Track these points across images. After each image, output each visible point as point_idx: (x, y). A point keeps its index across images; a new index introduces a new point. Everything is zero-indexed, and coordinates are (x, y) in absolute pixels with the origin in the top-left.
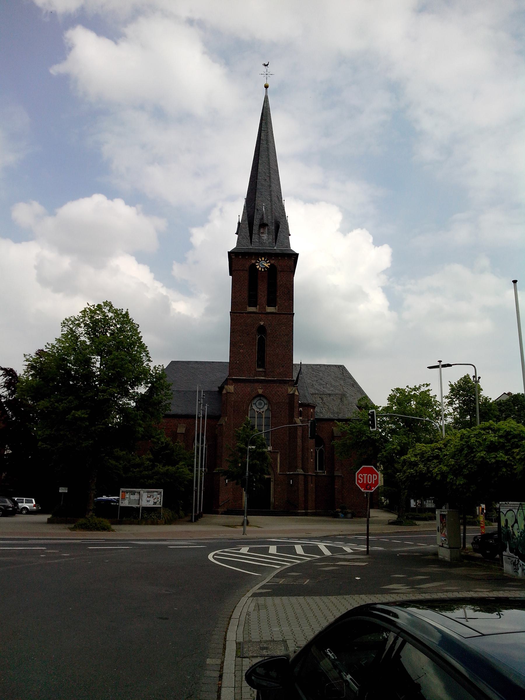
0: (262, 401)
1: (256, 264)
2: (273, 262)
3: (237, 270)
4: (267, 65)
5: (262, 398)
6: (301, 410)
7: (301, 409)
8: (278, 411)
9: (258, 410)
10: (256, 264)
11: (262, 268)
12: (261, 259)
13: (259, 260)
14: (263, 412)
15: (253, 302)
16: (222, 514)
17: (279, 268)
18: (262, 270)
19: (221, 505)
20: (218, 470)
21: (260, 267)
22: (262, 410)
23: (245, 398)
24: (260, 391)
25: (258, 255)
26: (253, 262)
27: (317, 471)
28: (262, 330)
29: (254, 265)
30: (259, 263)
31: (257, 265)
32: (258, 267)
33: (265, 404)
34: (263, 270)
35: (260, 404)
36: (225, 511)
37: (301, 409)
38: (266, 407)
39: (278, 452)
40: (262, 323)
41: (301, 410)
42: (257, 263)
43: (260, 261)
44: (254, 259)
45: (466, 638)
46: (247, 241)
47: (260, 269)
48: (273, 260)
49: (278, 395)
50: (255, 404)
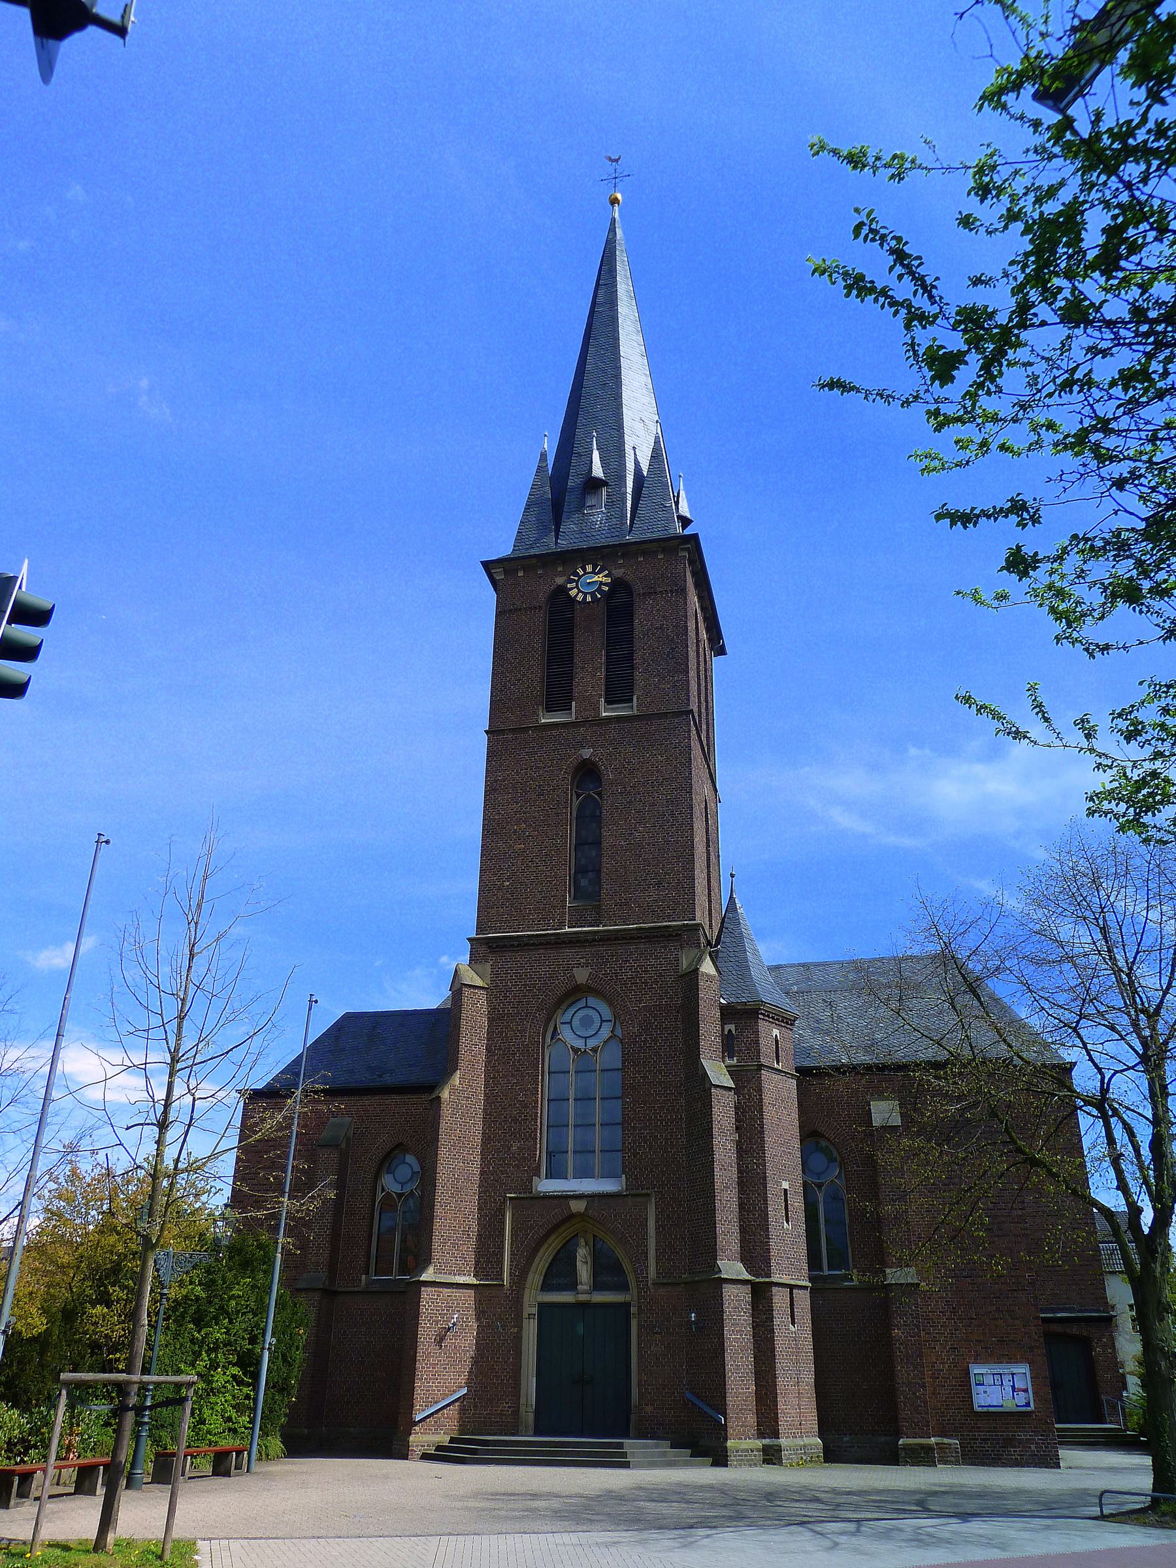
0: (591, 1012)
1: (569, 586)
2: (619, 573)
3: (511, 610)
4: (616, 161)
5: (592, 1001)
6: (730, 1031)
7: (732, 1027)
8: (645, 1041)
9: (579, 1044)
10: (569, 586)
11: (585, 594)
12: (584, 569)
13: (577, 574)
14: (594, 1050)
15: (558, 698)
16: (426, 1457)
17: (638, 588)
18: (585, 598)
19: (420, 1421)
20: (954, 1533)
21: (579, 591)
22: (592, 1043)
23: (528, 1003)
24: (582, 975)
25: (573, 558)
26: (560, 581)
27: (821, 1269)
28: (587, 773)
29: (562, 590)
30: (577, 582)
31: (572, 588)
32: (573, 593)
33: (602, 1021)
34: (589, 599)
35: (587, 1022)
36: (439, 1448)
37: (732, 1027)
38: (606, 1032)
39: (648, 1195)
40: (587, 753)
41: (730, 1031)
42: (572, 581)
43: (580, 577)
44: (561, 574)
45: (594, 1009)
46: (543, 530)
47: (580, 598)
48: (621, 566)
49: (646, 983)
50: (570, 1023)
